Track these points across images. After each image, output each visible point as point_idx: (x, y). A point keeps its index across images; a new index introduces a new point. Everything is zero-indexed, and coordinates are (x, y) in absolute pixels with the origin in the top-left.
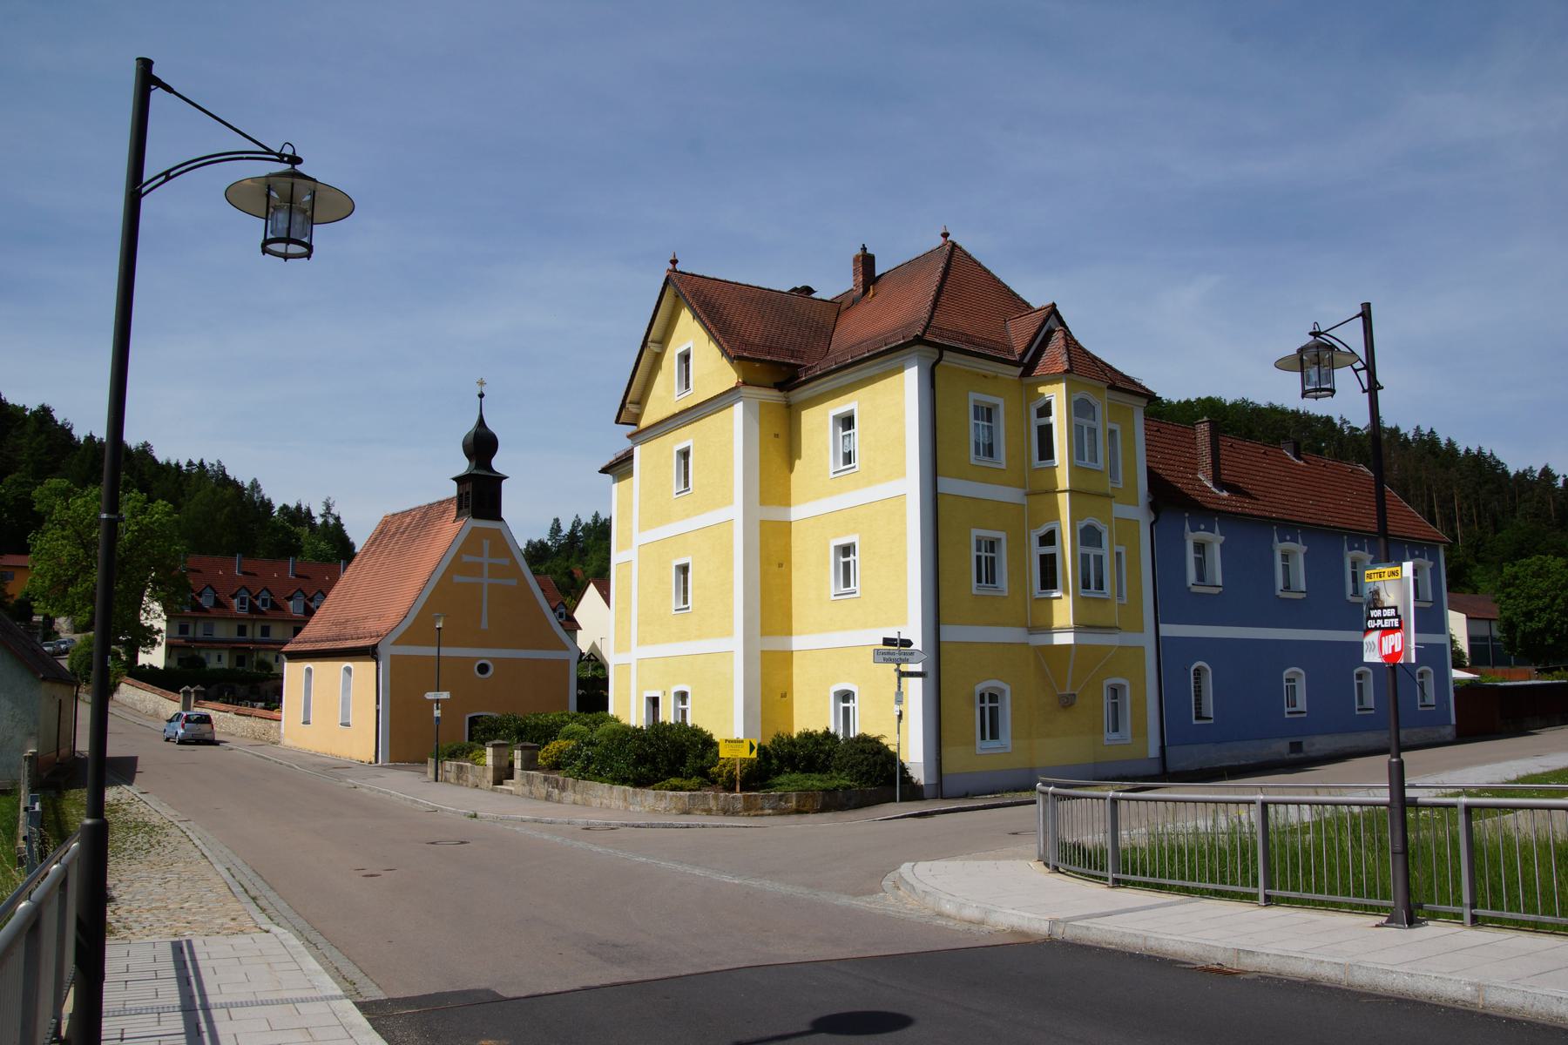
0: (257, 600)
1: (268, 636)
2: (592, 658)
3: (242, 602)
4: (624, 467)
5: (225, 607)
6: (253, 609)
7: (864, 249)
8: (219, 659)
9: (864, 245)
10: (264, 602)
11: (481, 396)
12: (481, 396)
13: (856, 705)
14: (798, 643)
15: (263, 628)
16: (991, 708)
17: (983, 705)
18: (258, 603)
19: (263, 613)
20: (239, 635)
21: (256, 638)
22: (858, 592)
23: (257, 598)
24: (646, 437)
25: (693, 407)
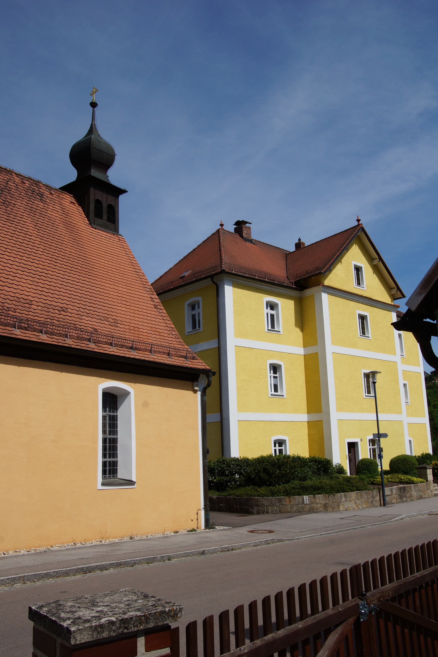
4: (276, 288)
7: (299, 240)
9: (299, 238)
11: (94, 105)
12: (94, 105)
13: (369, 447)
14: (304, 417)
16: (279, 450)
17: (275, 448)
22: (409, 403)
24: (340, 294)
25: (376, 300)
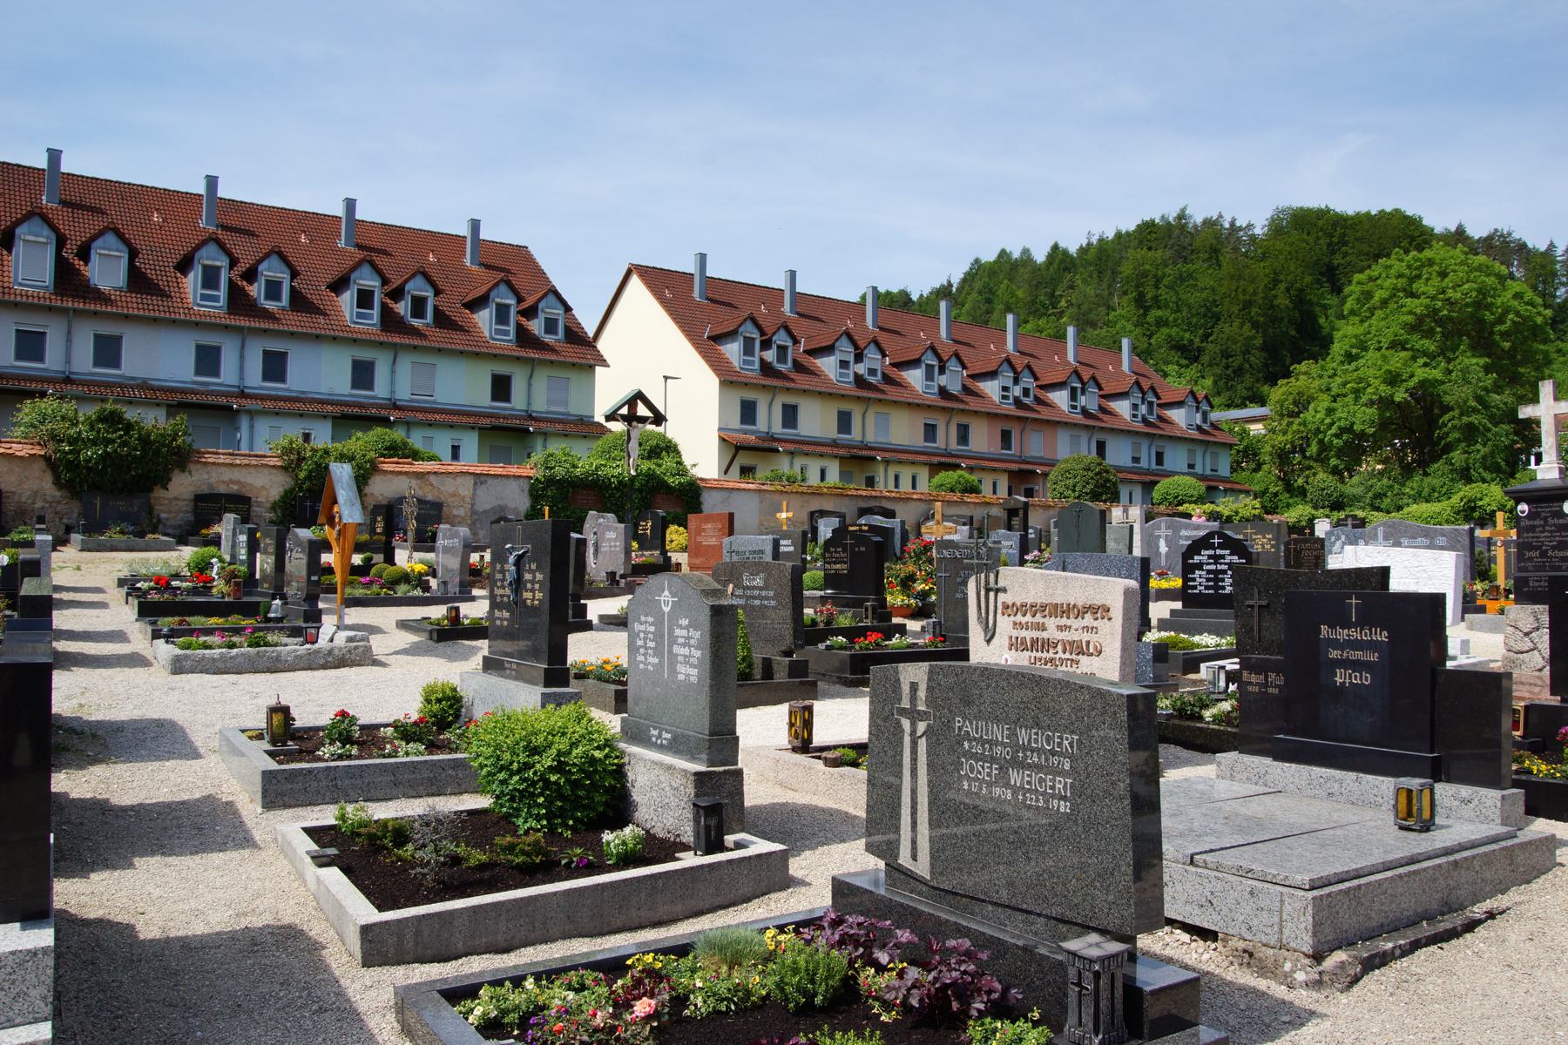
0: (251, 282)
1: (117, 365)
2: (642, 410)
3: (502, 314)
5: (461, 329)
6: (239, 301)
8: (456, 453)
10: (273, 290)
15: (267, 355)
18: (403, 308)
19: (415, 332)
20: (355, 385)
21: (398, 396)
23: (397, 294)
